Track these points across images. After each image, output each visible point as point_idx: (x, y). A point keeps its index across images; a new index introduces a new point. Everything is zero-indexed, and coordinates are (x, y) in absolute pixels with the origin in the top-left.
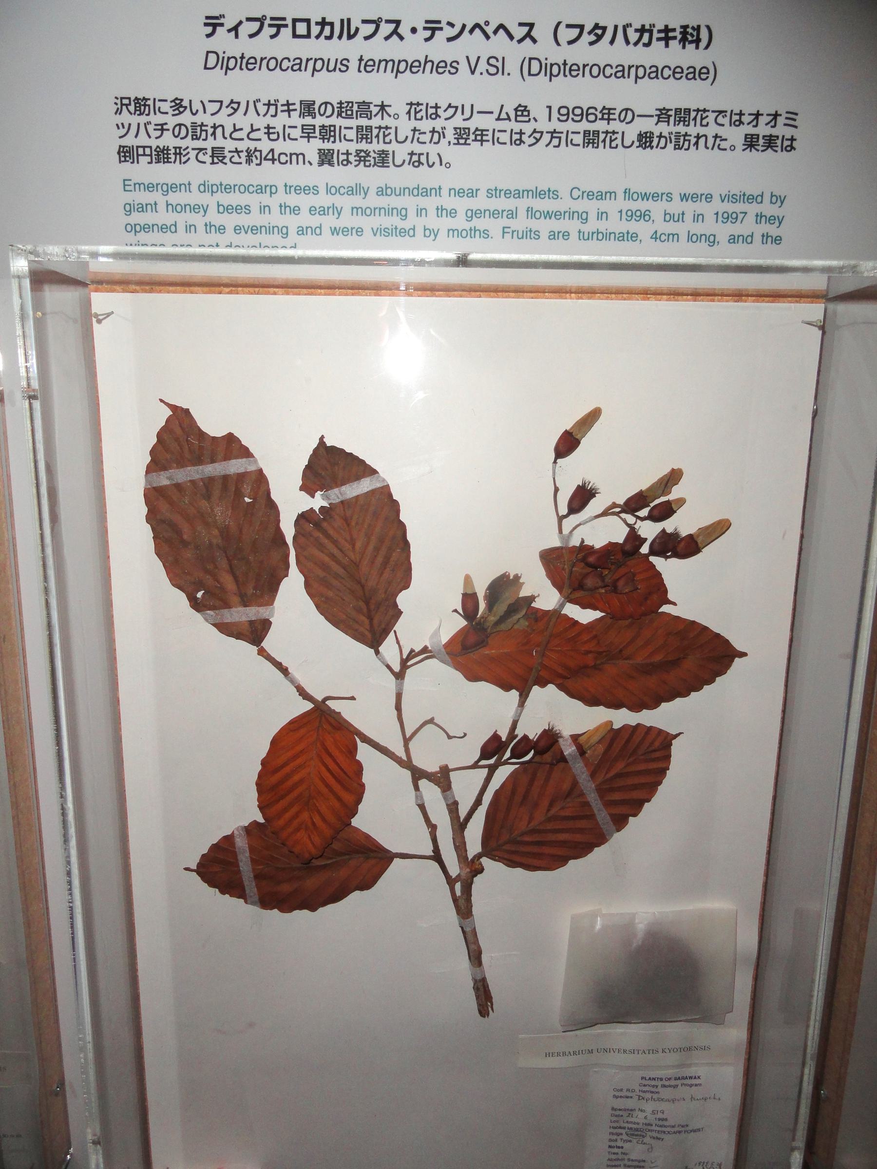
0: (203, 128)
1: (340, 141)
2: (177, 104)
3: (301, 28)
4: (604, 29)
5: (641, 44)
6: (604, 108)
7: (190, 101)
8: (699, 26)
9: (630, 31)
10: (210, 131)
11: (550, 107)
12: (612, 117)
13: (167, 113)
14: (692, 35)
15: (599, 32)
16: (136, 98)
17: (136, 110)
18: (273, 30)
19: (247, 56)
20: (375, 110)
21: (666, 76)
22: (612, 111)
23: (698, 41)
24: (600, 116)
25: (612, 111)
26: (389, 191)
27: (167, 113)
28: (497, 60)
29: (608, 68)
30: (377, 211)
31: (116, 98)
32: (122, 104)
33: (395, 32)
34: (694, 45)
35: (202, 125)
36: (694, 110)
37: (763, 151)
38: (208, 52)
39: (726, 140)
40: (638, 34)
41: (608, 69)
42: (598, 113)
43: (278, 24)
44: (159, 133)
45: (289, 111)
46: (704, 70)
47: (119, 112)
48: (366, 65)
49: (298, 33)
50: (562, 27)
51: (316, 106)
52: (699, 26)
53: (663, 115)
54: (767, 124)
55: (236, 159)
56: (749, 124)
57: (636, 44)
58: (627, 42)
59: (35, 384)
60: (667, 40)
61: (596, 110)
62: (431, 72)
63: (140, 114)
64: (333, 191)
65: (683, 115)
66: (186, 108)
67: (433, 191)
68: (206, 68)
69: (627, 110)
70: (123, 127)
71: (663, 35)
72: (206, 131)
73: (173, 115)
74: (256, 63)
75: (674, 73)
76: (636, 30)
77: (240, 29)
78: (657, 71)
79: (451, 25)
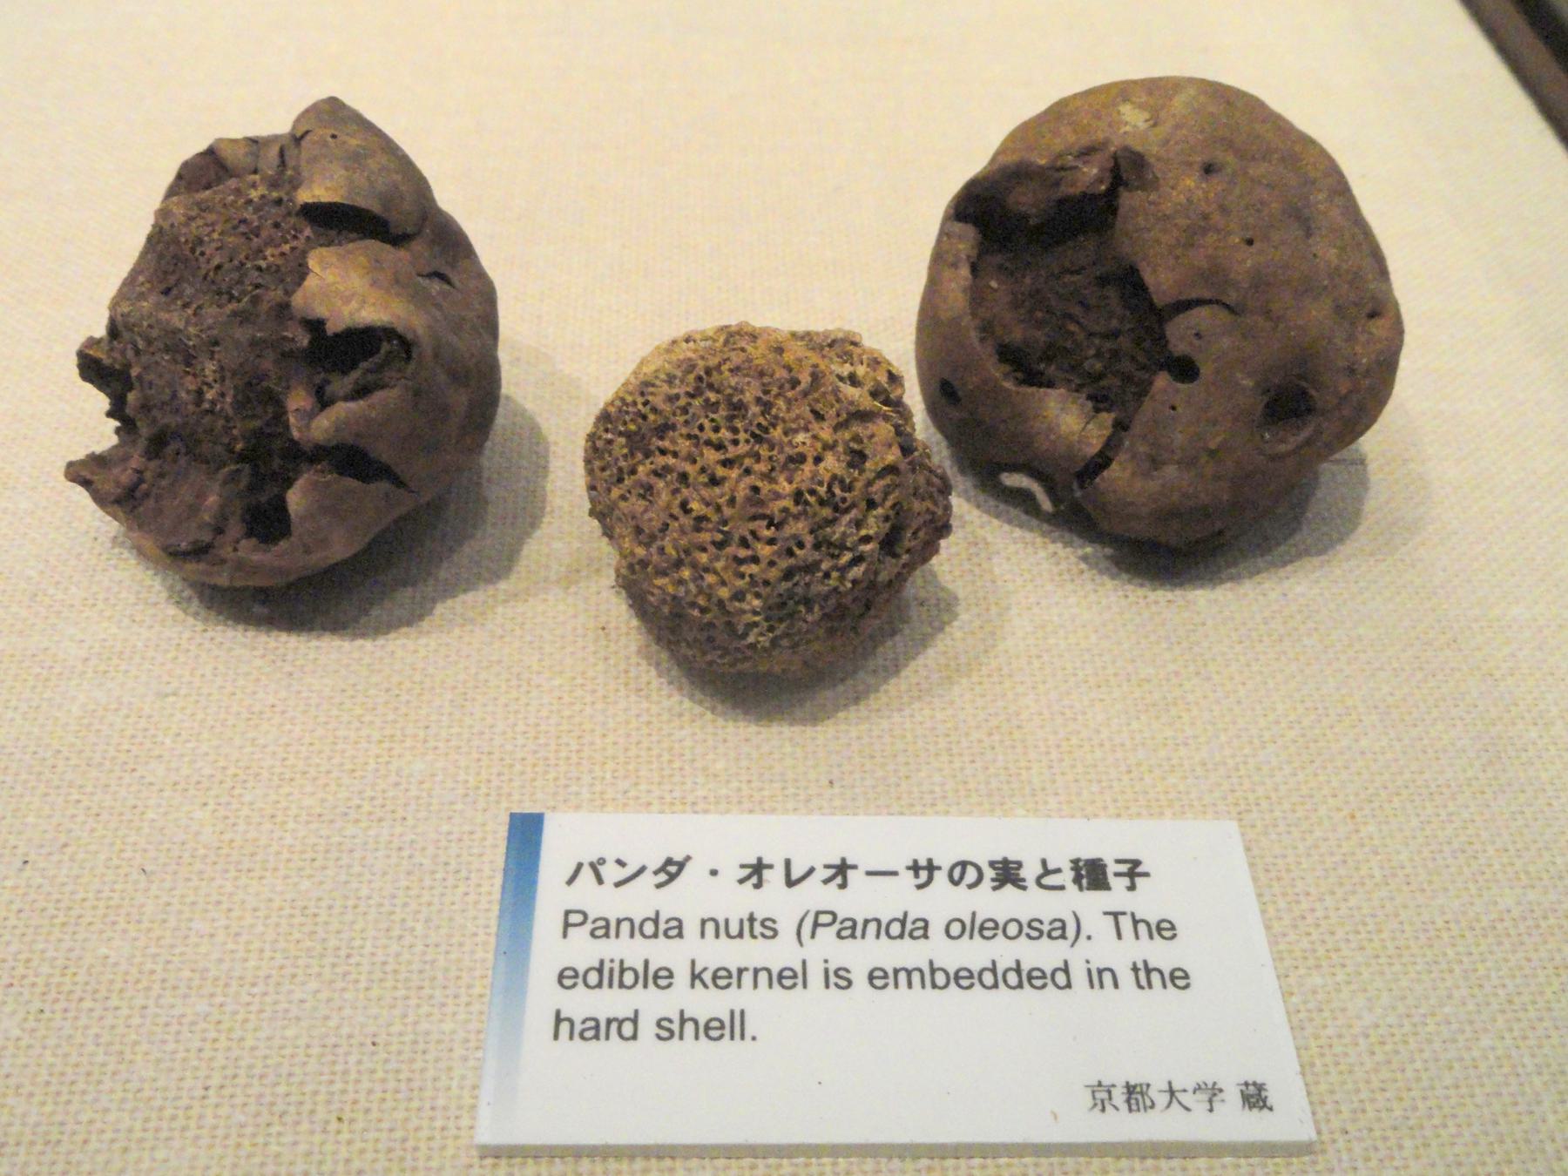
15: (673, 869)
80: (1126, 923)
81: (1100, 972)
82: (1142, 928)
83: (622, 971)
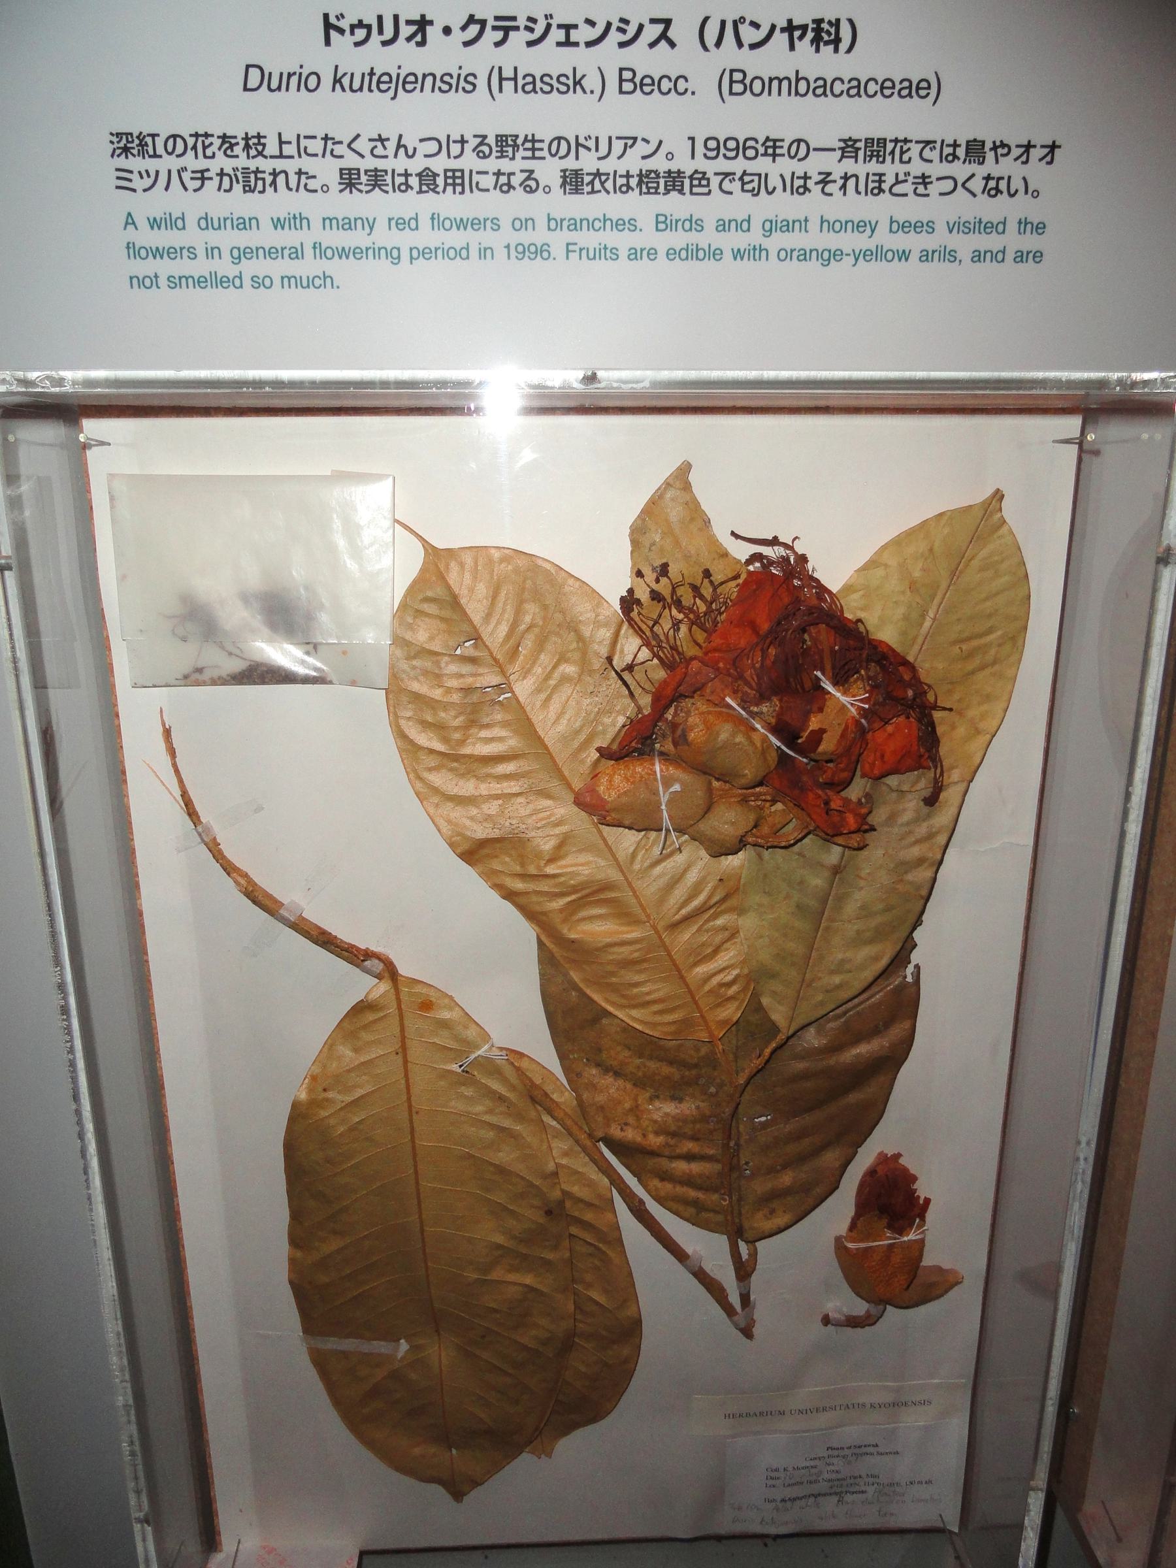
0: (259, 175)
1: (471, 191)
5: (413, 43)
6: (767, 139)
8: (838, 21)
10: (269, 179)
11: (692, 139)
12: (778, 151)
14: (829, 33)
18: (499, 35)
19: (378, 72)
21: (871, 92)
22: (778, 144)
23: (837, 41)
24: (762, 150)
25: (778, 144)
29: (837, 83)
31: (112, 134)
33: (664, 36)
34: (831, 47)
36: (891, 141)
37: (367, 192)
38: (248, 67)
39: (314, 177)
40: (786, 35)
41: (837, 84)
42: (759, 146)
43: (506, 26)
44: (199, 183)
48: (379, 82)
52: (838, 21)
53: (849, 148)
54: (1041, 160)
61: (757, 142)
62: (298, 90)
65: (876, 148)
68: (246, 89)
69: (799, 141)
70: (149, 176)
72: (263, 179)
74: (416, 82)
75: (882, 88)
78: (825, 86)
79: (591, 23)
81: (212, 249)
83: (697, 250)
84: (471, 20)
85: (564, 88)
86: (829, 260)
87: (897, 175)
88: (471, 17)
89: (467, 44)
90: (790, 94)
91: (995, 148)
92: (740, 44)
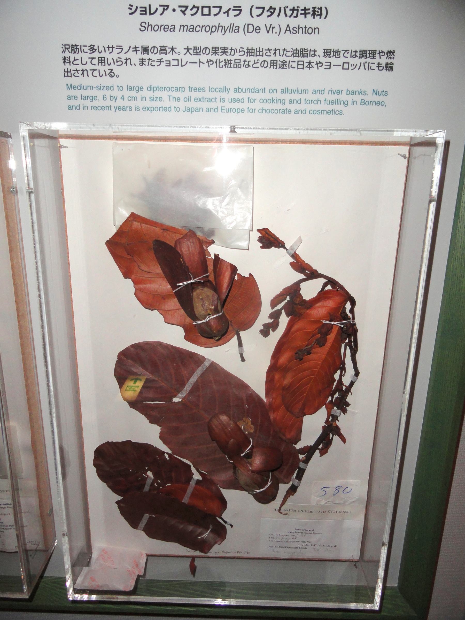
2: (91, 48)
3: (206, 11)
4: (275, 9)
5: (293, 17)
7: (98, 46)
8: (321, 7)
9: (287, 10)
13: (87, 52)
14: (318, 12)
15: (272, 10)
16: (72, 45)
17: (72, 51)
19: (308, 27)
20: (169, 50)
21: (197, 30)
23: (321, 15)
26: (240, 90)
27: (87, 52)
28: (146, 24)
30: (372, 103)
31: (292, 49)
32: (66, 47)
35: (230, 60)
40: (291, 12)
44: (159, 63)
45: (136, 51)
46: (258, 28)
47: (64, 52)
49: (208, 13)
50: (254, 8)
51: (149, 49)
52: (321, 7)
55: (76, 74)
56: (291, 56)
57: (290, 16)
58: (286, 16)
59: (32, 186)
60: (305, 14)
62: (151, 30)
63: (74, 53)
64: (213, 90)
66: (96, 50)
67: (261, 90)
71: (303, 12)
73: (90, 53)
76: (290, 10)
77: (230, 12)
80: (171, 98)
82: (174, 99)
84: (194, 7)
85: (295, 32)
86: (138, 90)
87: (255, 61)
88: (194, 6)
89: (192, 15)
90: (302, 33)
91: (379, 53)
92: (286, 16)
